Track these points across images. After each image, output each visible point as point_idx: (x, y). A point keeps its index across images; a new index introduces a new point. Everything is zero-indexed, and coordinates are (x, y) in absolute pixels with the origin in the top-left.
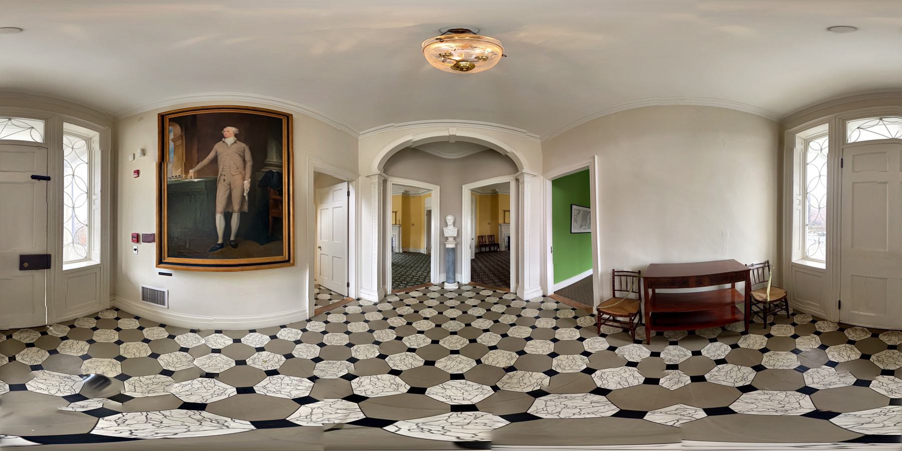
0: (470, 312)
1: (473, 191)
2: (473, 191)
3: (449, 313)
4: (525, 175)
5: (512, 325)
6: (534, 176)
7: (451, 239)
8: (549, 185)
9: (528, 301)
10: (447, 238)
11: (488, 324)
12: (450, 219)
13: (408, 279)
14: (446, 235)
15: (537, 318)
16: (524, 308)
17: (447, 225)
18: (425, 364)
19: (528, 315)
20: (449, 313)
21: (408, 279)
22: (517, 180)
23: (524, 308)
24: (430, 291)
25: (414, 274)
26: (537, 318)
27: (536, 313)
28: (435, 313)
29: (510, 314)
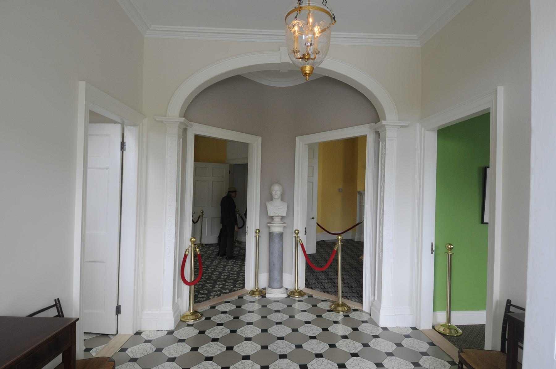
0: (302, 330)
1: (311, 147)
2: (311, 147)
3: (276, 331)
4: (387, 128)
5: (355, 355)
6: (406, 127)
7: (277, 220)
8: (431, 141)
9: (385, 329)
10: (272, 218)
11: (322, 347)
12: (277, 190)
13: (214, 277)
14: (271, 214)
15: (390, 354)
16: (376, 337)
17: (271, 198)
18: (231, 332)
19: (377, 348)
20: (276, 331)
21: (214, 277)
22: (377, 133)
23: (376, 337)
24: (271, 312)
25: (220, 270)
26: (390, 354)
27: (390, 347)
28: (258, 331)
29: (356, 340)
